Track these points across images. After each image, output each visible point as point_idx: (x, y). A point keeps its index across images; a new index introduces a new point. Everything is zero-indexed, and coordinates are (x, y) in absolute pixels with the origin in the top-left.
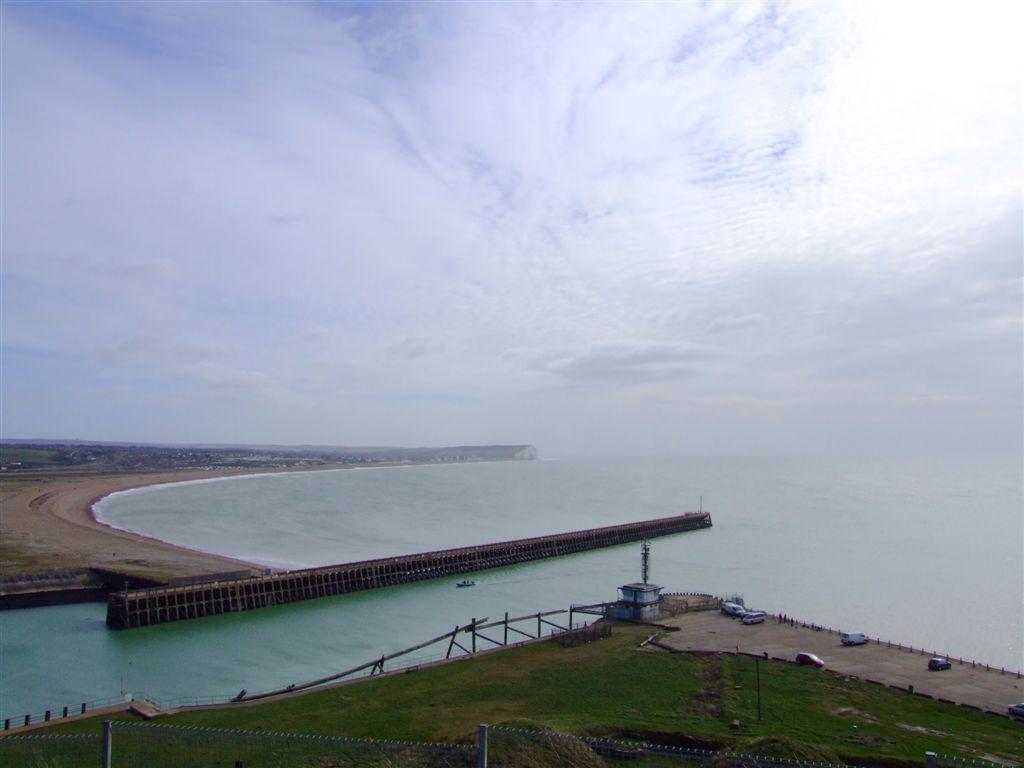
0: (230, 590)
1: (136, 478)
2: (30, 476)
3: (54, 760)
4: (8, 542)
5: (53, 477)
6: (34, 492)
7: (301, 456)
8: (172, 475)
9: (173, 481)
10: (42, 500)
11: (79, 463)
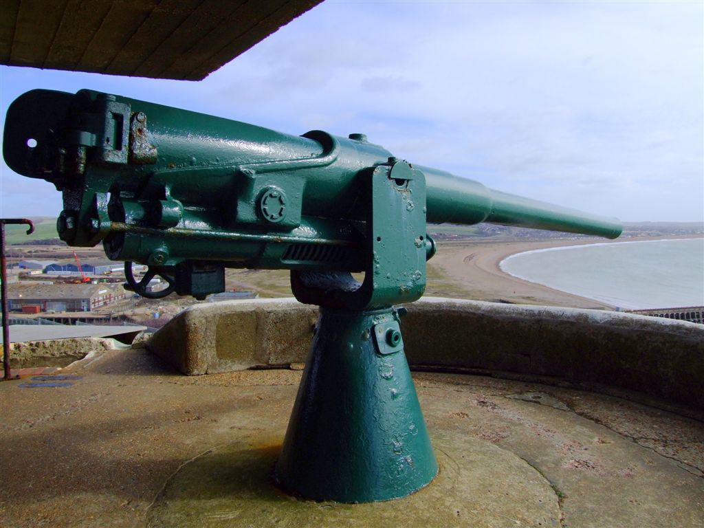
0: (696, 314)
1: (525, 245)
2: (463, 243)
3: (626, 489)
4: (453, 282)
5: (475, 244)
6: (467, 252)
7: (642, 229)
8: (550, 243)
9: (566, 246)
10: (470, 258)
11: (491, 235)
